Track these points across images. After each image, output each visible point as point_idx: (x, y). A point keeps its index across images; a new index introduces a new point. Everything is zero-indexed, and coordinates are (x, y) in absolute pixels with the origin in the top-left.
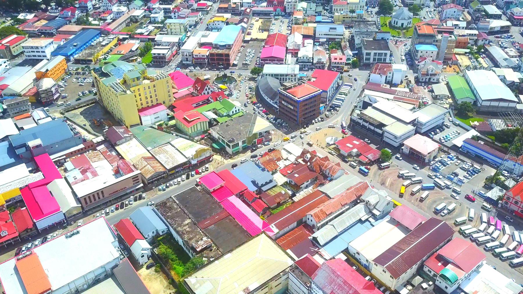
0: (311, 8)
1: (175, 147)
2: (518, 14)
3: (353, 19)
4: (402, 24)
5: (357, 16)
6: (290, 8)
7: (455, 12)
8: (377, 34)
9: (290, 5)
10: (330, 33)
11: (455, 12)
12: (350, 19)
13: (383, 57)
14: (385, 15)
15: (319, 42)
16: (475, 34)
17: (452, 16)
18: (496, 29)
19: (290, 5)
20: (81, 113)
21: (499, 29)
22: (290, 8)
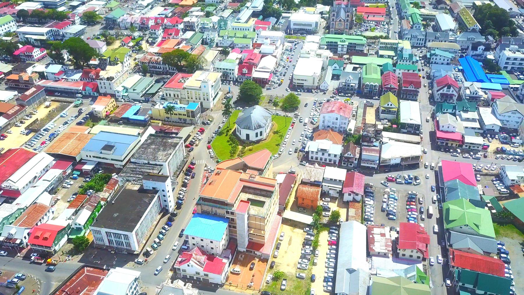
0: (134, 90)
1: (42, 194)
2: (445, 129)
3: (181, 117)
4: (248, 136)
5: (186, 113)
6: (103, 87)
7: (337, 119)
8: (109, 194)
9: (102, 84)
10: (102, 156)
11: (337, 119)
12: (178, 116)
13: (113, 238)
14: (243, 108)
15: (81, 170)
16: (340, 181)
17: (333, 124)
18: (392, 162)
19: (102, 84)
20: (232, 264)
21: (398, 161)
22: (103, 87)
